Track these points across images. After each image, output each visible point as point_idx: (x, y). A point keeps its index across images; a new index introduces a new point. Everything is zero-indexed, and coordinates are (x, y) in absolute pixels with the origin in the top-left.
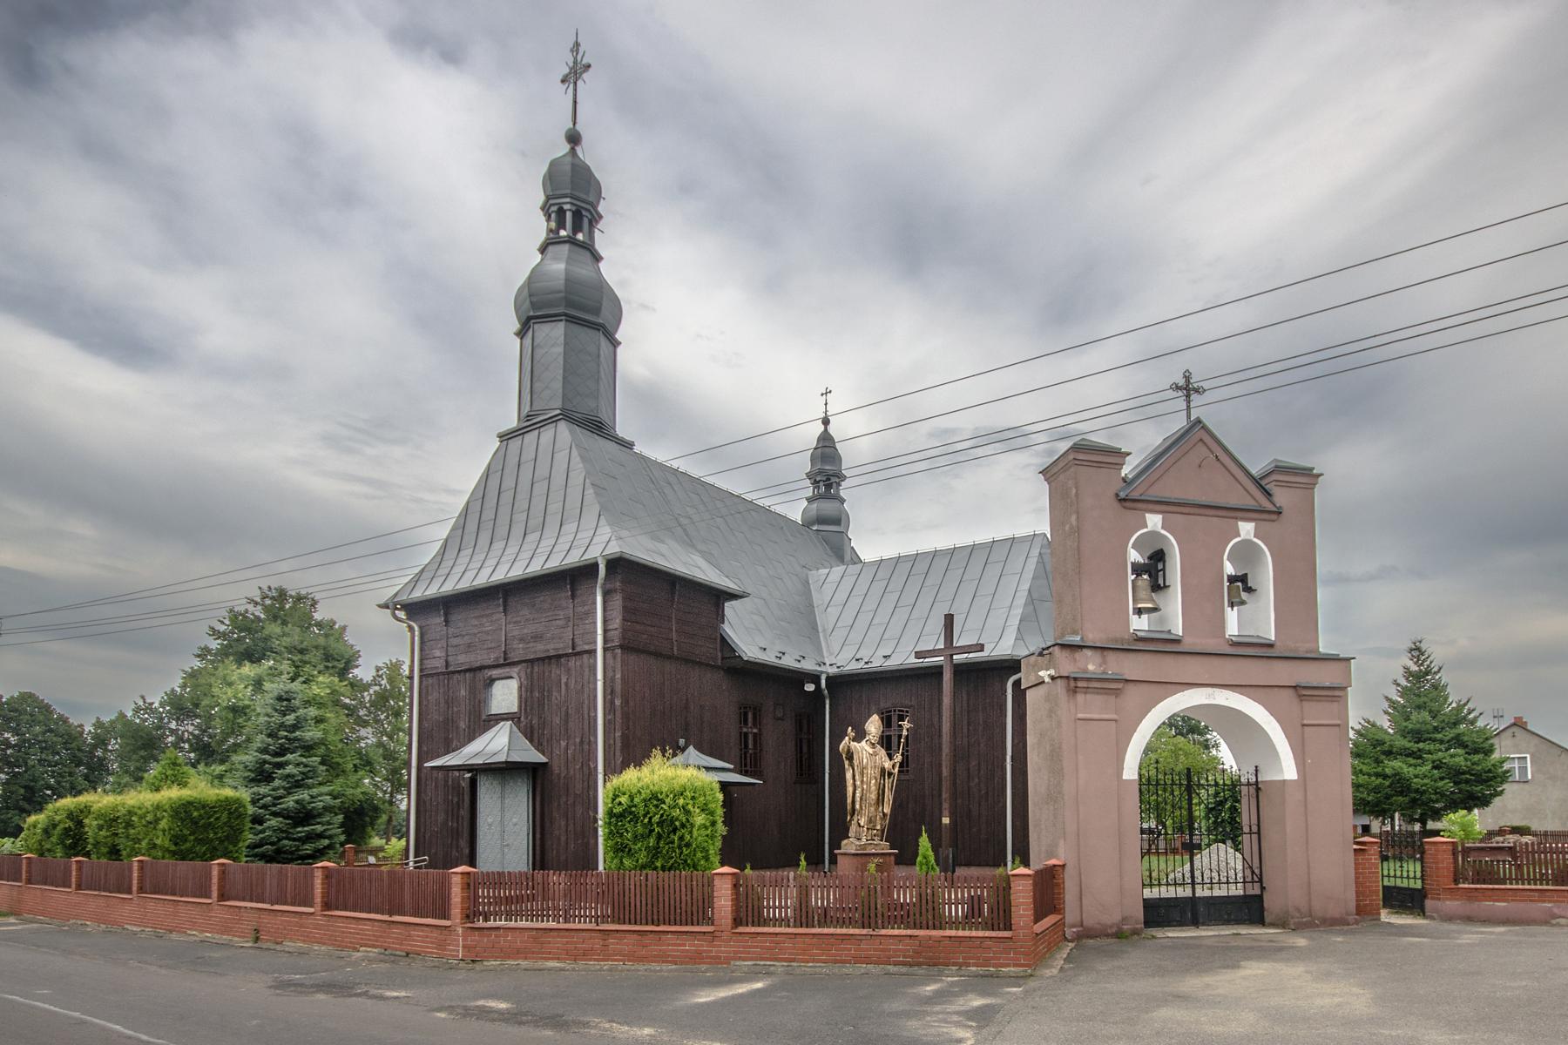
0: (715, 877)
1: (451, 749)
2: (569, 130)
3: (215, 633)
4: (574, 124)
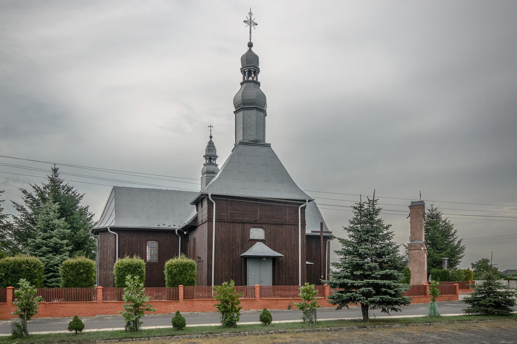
0: (7, 289)
1: (245, 251)
2: (249, 43)
3: (459, 242)
4: (250, 40)
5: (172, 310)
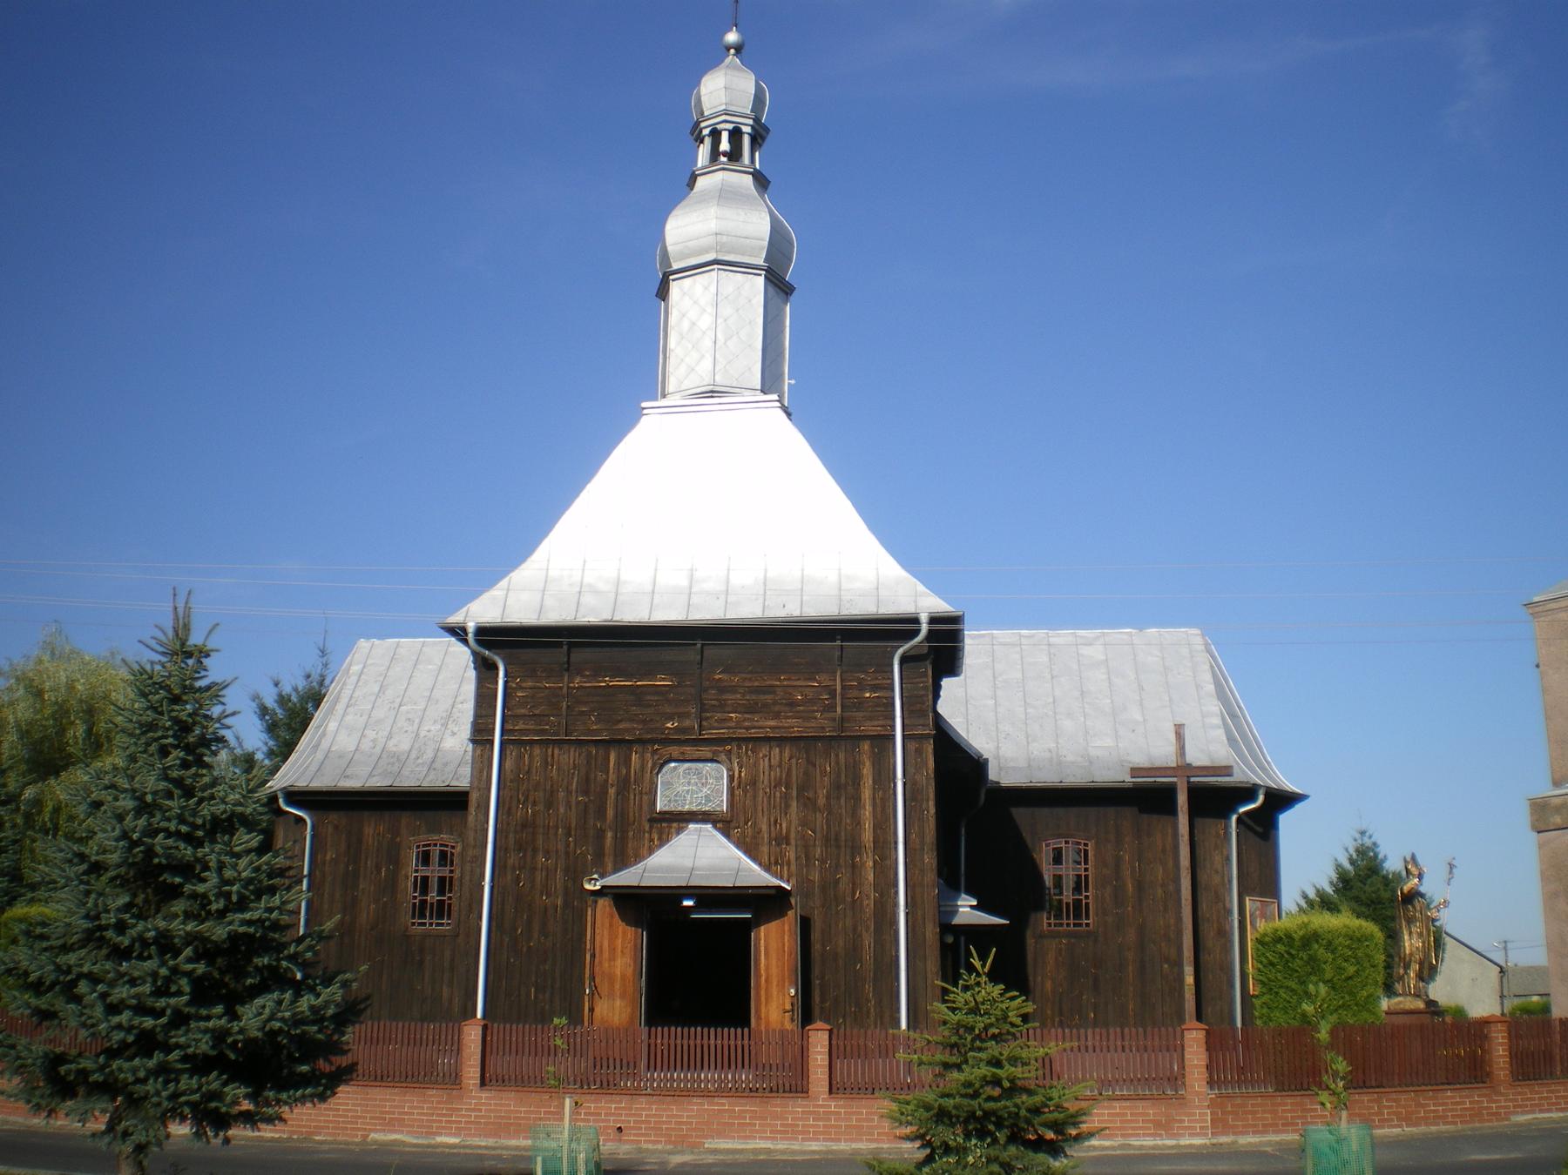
5: (635, 1135)
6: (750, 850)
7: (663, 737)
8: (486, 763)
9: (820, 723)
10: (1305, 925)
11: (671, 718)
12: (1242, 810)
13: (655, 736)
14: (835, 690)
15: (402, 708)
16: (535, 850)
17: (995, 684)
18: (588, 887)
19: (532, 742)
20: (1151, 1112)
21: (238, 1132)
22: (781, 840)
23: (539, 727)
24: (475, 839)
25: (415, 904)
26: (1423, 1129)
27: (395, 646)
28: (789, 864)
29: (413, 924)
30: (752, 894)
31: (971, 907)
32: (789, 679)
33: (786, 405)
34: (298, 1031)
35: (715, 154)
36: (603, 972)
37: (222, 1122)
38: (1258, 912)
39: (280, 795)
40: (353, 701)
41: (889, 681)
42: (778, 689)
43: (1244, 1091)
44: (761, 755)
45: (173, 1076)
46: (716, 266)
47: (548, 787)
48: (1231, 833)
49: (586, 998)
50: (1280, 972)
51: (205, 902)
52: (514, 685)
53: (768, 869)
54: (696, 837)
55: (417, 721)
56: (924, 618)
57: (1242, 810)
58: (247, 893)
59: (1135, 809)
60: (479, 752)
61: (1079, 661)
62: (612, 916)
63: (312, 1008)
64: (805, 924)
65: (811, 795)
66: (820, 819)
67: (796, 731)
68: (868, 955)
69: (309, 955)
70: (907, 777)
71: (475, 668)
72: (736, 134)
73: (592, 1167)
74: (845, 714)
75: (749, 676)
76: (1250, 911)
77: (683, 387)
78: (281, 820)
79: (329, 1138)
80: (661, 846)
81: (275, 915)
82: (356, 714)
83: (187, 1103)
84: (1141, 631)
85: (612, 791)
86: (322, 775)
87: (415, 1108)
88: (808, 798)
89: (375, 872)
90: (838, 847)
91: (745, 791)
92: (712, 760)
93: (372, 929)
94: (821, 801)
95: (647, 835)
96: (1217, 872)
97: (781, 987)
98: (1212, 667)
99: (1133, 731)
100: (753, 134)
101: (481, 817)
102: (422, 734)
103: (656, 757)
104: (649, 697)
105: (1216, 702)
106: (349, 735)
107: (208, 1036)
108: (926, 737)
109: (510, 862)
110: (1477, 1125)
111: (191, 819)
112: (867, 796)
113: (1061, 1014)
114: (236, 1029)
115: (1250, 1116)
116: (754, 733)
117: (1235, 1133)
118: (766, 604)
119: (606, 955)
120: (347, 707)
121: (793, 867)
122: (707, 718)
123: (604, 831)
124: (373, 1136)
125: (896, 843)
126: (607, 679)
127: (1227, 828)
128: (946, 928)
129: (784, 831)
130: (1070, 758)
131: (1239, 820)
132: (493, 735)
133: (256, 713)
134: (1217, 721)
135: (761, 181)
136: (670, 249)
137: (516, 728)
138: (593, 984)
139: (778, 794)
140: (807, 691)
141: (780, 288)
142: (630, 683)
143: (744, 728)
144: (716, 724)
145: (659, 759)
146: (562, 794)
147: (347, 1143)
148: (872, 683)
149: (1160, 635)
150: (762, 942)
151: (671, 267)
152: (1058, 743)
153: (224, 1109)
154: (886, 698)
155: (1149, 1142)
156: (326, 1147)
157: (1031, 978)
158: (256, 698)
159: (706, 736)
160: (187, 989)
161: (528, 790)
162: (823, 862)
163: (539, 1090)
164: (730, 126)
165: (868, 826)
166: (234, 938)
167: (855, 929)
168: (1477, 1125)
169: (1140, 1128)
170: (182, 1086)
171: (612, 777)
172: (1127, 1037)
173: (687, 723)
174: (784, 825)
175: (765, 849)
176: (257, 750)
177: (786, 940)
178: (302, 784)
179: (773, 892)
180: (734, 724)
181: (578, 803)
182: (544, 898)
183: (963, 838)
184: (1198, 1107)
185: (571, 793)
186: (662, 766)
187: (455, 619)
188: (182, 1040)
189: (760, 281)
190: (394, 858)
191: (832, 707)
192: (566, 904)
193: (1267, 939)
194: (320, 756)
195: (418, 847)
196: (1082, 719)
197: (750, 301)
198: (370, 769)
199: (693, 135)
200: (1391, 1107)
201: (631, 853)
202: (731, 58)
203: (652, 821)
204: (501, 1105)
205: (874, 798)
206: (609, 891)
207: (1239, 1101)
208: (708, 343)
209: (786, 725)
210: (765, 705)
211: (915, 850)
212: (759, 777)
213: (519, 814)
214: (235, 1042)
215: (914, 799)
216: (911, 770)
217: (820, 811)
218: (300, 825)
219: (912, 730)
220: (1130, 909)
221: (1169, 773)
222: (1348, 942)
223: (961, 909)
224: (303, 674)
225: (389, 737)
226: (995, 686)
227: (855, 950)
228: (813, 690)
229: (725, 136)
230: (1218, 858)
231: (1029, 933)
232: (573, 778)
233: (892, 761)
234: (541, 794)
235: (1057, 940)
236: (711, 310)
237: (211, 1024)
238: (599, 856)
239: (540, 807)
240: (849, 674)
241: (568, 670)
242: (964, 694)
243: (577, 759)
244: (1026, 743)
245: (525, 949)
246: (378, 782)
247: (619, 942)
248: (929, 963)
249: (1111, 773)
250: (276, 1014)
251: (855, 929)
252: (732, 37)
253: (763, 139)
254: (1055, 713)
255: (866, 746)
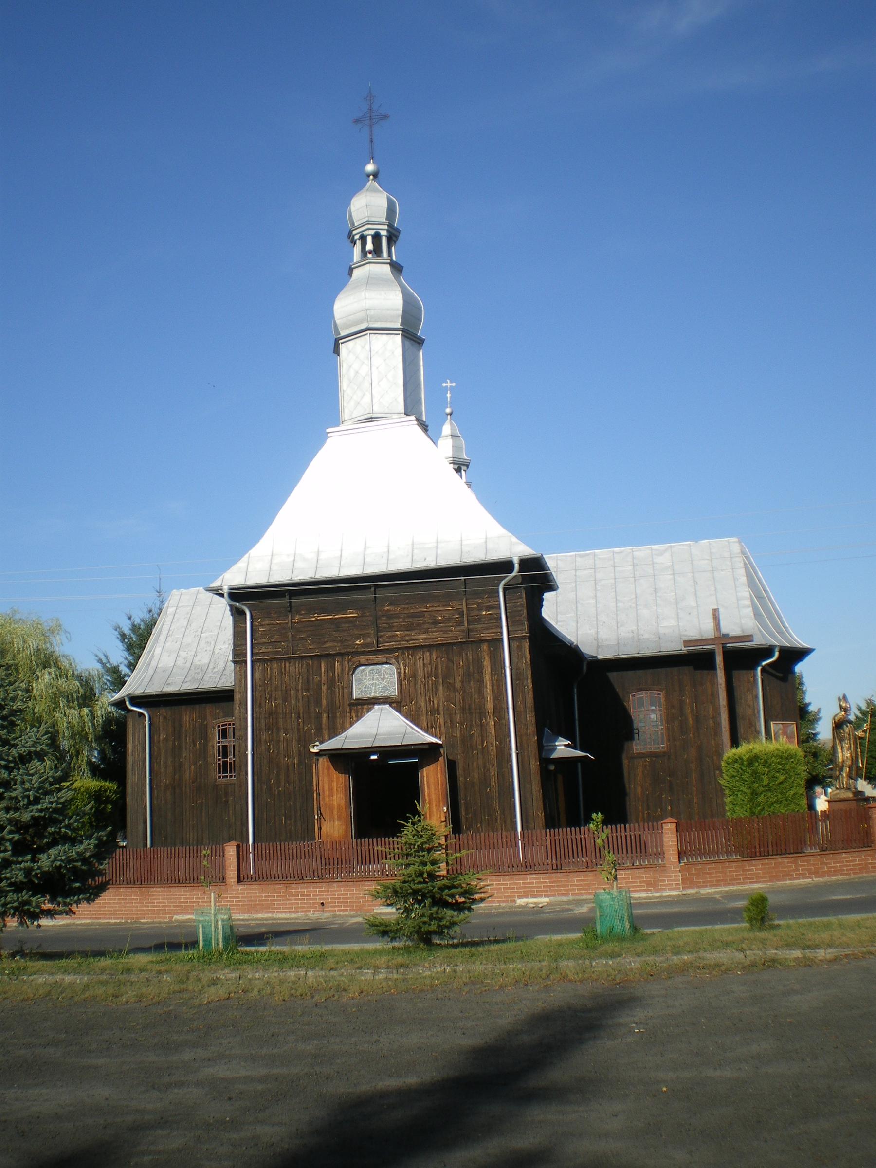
5: (332, 907)
6: (414, 718)
7: (354, 650)
8: (243, 674)
9: (455, 634)
10: (751, 750)
11: (359, 638)
12: (764, 663)
13: (349, 650)
14: (463, 611)
15: (202, 635)
16: (278, 729)
17: (596, 588)
18: (312, 750)
19: (271, 660)
20: (644, 876)
21: (45, 922)
22: (434, 711)
23: (275, 650)
24: (240, 725)
25: (219, 764)
26: (827, 879)
27: (196, 593)
28: (440, 727)
29: (220, 777)
30: (414, 749)
31: (565, 745)
32: (433, 607)
33: (424, 420)
34: (70, 866)
35: (364, 252)
36: (325, 804)
37: (35, 916)
38: (780, 732)
39: (126, 699)
40: (171, 632)
41: (497, 603)
42: (426, 614)
43: (704, 860)
44: (418, 657)
45: (4, 894)
46: (368, 332)
47: (284, 688)
48: (757, 679)
49: (316, 821)
50: (738, 781)
51: (17, 801)
52: (257, 624)
53: (427, 731)
54: (379, 714)
55: (213, 643)
56: (516, 561)
57: (764, 663)
58: (38, 795)
59: (691, 668)
60: (238, 669)
61: (653, 567)
62: (329, 768)
63: (78, 853)
64: (452, 766)
65: (451, 681)
66: (458, 696)
67: (440, 640)
68: (494, 782)
69: (76, 824)
70: (513, 666)
71: (232, 615)
72: (377, 237)
73: (228, 930)
74: (470, 627)
75: (407, 606)
76: (774, 731)
77: (354, 416)
78: (130, 714)
79: (150, 921)
80: (357, 720)
81: (54, 805)
82: (173, 641)
83: (12, 907)
84: (697, 542)
85: (324, 688)
86: (153, 684)
87: (199, 898)
88: (449, 683)
89: (192, 745)
90: (471, 714)
91: (409, 682)
92: (387, 663)
93: (193, 782)
94: (458, 685)
95: (348, 714)
96: (749, 706)
97: (438, 806)
98: (745, 564)
99: (690, 614)
100: (388, 235)
101: (243, 710)
102: (216, 652)
103: (351, 664)
104: (343, 625)
105: (747, 589)
106: (169, 656)
107: (22, 872)
108: (523, 638)
109: (263, 737)
110: (865, 875)
111: (7, 758)
112: (487, 679)
113: (648, 808)
114: (36, 867)
115: (708, 876)
116: (413, 644)
117: (698, 887)
118: (414, 558)
119: (327, 793)
120: (167, 637)
121: (443, 728)
122: (381, 636)
123: (321, 714)
124: (176, 917)
125: (508, 708)
126: (316, 615)
127: (755, 676)
128: (545, 761)
129: (436, 706)
130: (646, 636)
131: (763, 671)
132: (246, 657)
133: (118, 638)
134: (748, 602)
135: (397, 268)
136: (338, 322)
137: (261, 651)
138: (319, 812)
139: (430, 682)
140: (444, 613)
141: (414, 340)
142: (331, 617)
143: (406, 641)
144: (387, 640)
145: (353, 665)
146: (292, 692)
147: (160, 923)
148: (487, 605)
149: (710, 544)
150: (425, 778)
151: (340, 334)
152: (638, 626)
153: (32, 909)
154: (496, 614)
155: (643, 895)
156: (146, 926)
157: (627, 786)
158: (117, 628)
159: (381, 648)
160: (10, 848)
161: (271, 691)
162: (462, 724)
163: (273, 883)
164: (372, 232)
165: (489, 698)
166: (33, 818)
167: (485, 767)
168: (865, 875)
169: (638, 886)
170: (9, 899)
171: (324, 678)
172: (628, 830)
173: (369, 640)
174: (435, 702)
175: (424, 718)
176: (121, 663)
177: (439, 776)
178: (140, 691)
179: (427, 746)
180: (399, 639)
181: (303, 697)
182: (286, 759)
183: (576, 696)
184: (673, 872)
185: (299, 691)
186: (355, 669)
187: (216, 584)
188: (8, 875)
189: (399, 339)
190: (204, 736)
191: (461, 623)
192: (300, 762)
193: (730, 760)
194: (151, 671)
195: (219, 727)
196: (655, 608)
197: (393, 353)
198: (184, 678)
199: (349, 239)
200: (804, 865)
201: (339, 726)
202: (371, 183)
203: (350, 705)
204: (251, 893)
205: (492, 680)
206: (324, 753)
207: (700, 866)
208: (367, 384)
209: (433, 637)
210: (418, 625)
211: (521, 712)
212: (418, 672)
213: (266, 706)
214: (37, 874)
215: (518, 679)
216: (515, 660)
217: (458, 691)
218: (142, 717)
219: (514, 634)
220: (691, 735)
221: (710, 642)
222: (778, 760)
223: (558, 748)
224: (141, 617)
225: (195, 655)
226: (596, 590)
227: (485, 780)
228: (450, 612)
229: (369, 240)
230: (750, 697)
231: (624, 756)
232: (299, 681)
233: (502, 655)
234: (280, 693)
235: (643, 759)
236: (367, 362)
237: (22, 866)
238: (319, 729)
239: (279, 701)
240: (471, 600)
241: (290, 611)
242: (575, 596)
243: (300, 668)
244: (616, 628)
245: (276, 793)
246: (189, 686)
247: (335, 784)
248: (533, 784)
249: (672, 646)
250: (57, 858)
251: (485, 767)
252: (370, 168)
253: (397, 237)
254: (637, 605)
255: (485, 647)
